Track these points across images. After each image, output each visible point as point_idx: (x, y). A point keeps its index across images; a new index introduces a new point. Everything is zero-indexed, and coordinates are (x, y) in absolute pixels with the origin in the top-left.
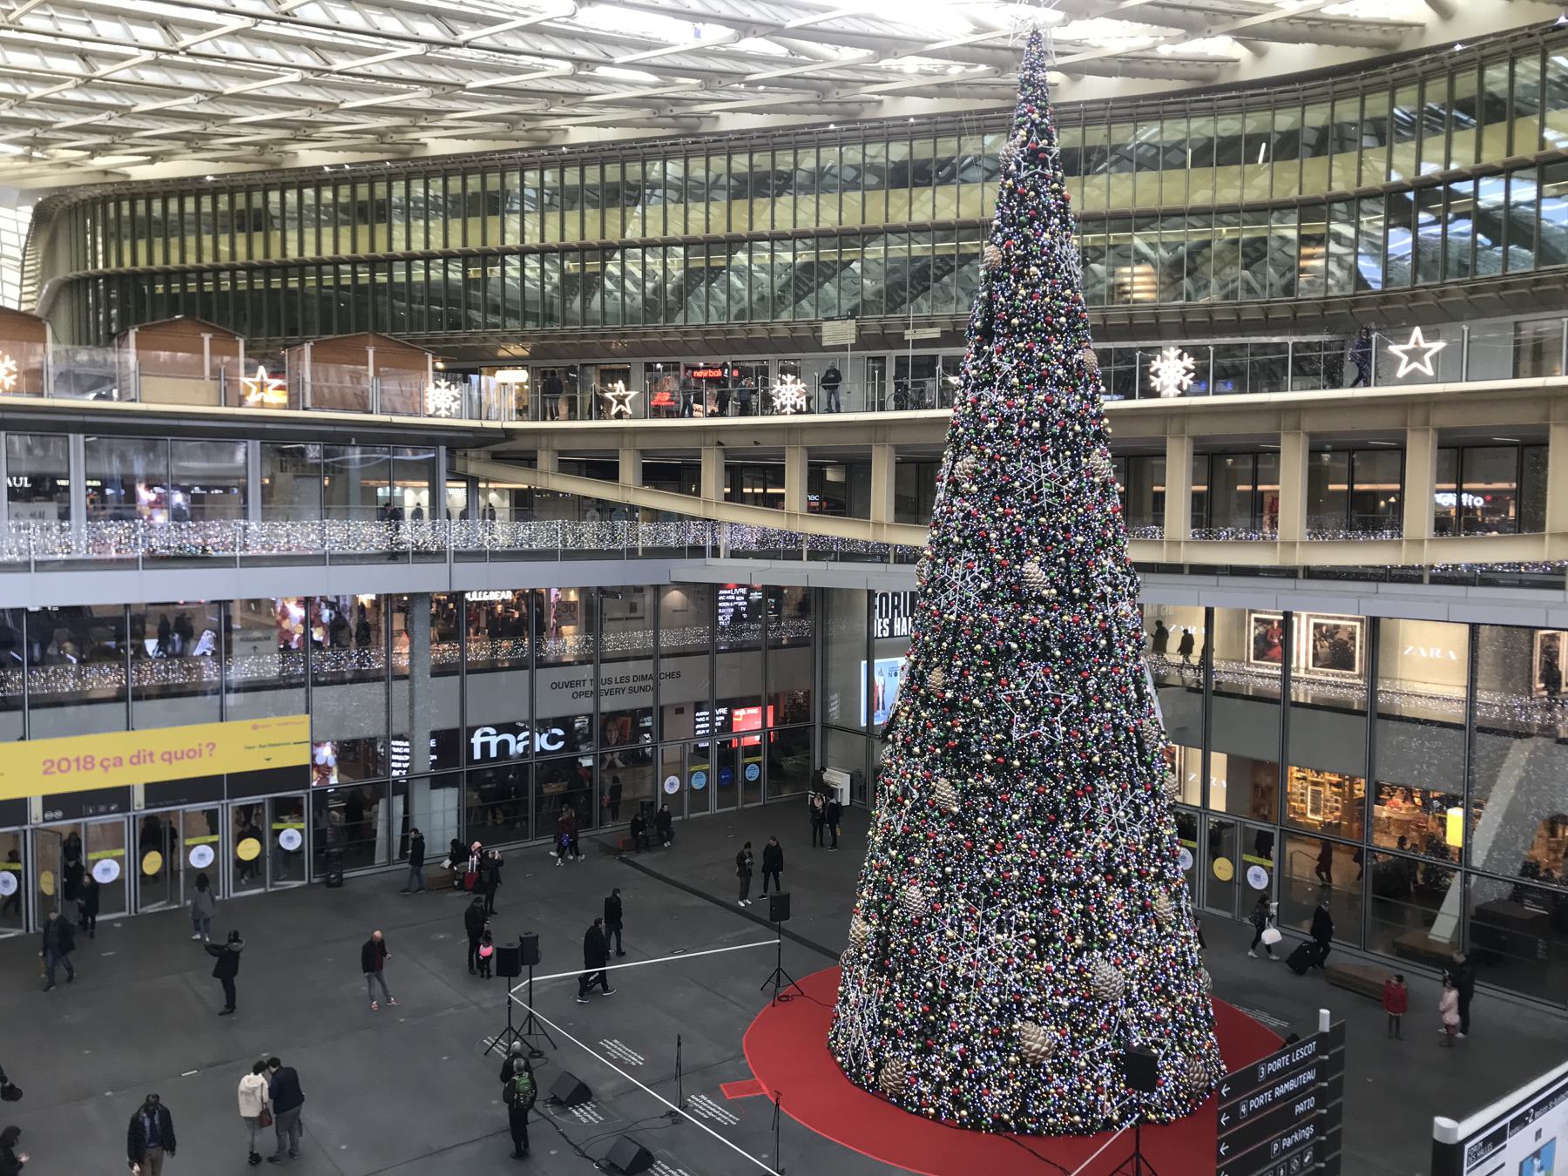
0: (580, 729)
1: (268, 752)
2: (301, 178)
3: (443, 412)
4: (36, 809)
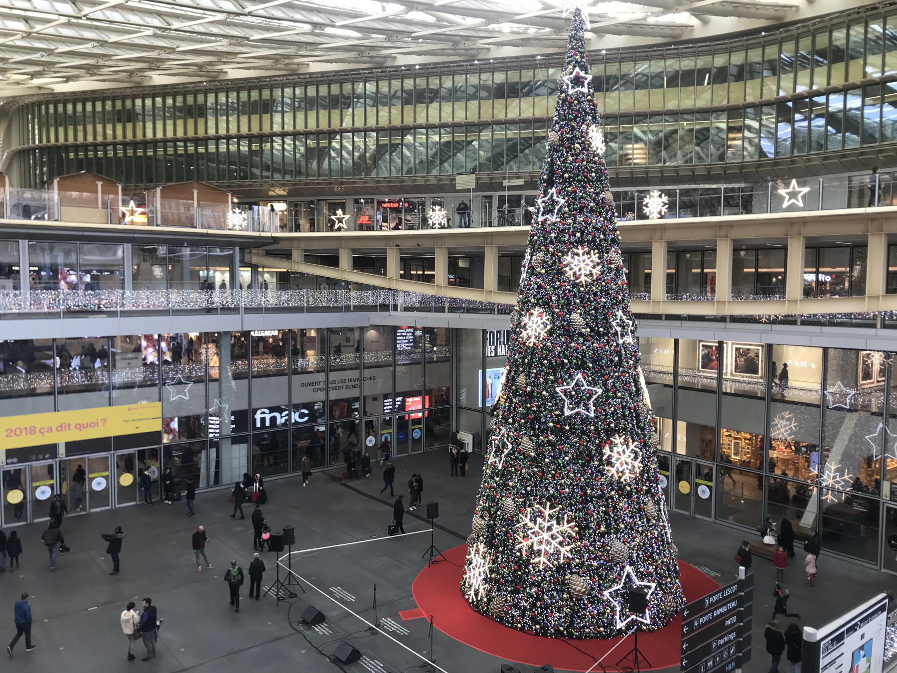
0: (318, 409)
1: (137, 424)
3: (237, 227)
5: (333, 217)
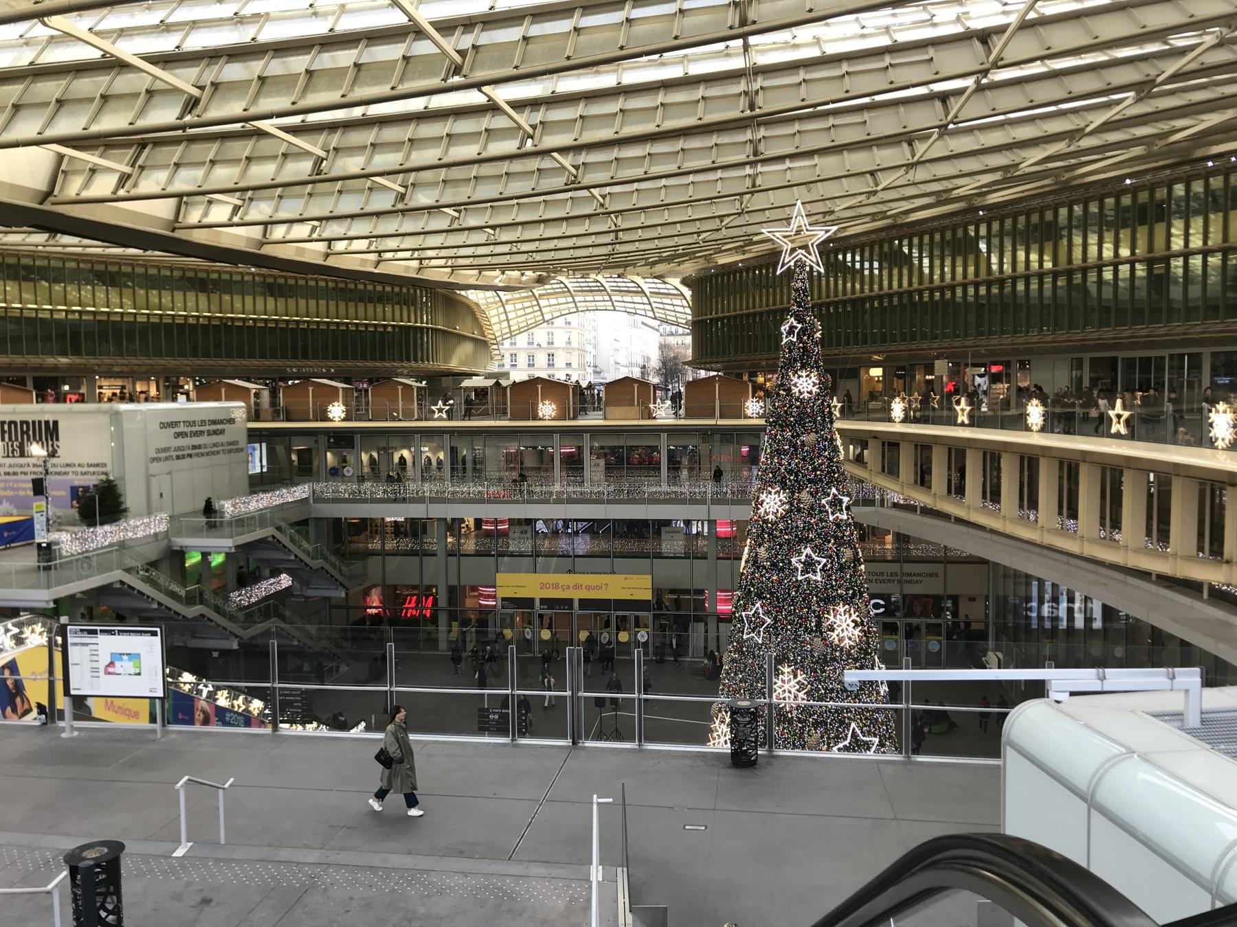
0: (895, 602)
1: (517, 590)
2: (1071, 198)
3: (337, 419)
4: (537, 603)
5: (433, 408)
